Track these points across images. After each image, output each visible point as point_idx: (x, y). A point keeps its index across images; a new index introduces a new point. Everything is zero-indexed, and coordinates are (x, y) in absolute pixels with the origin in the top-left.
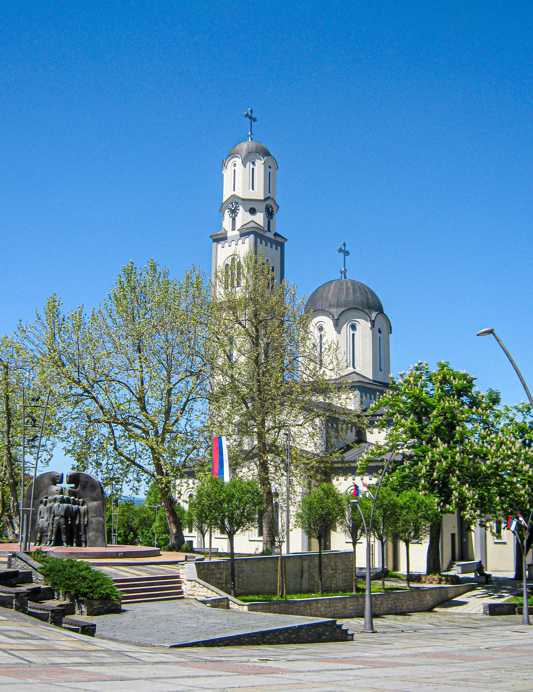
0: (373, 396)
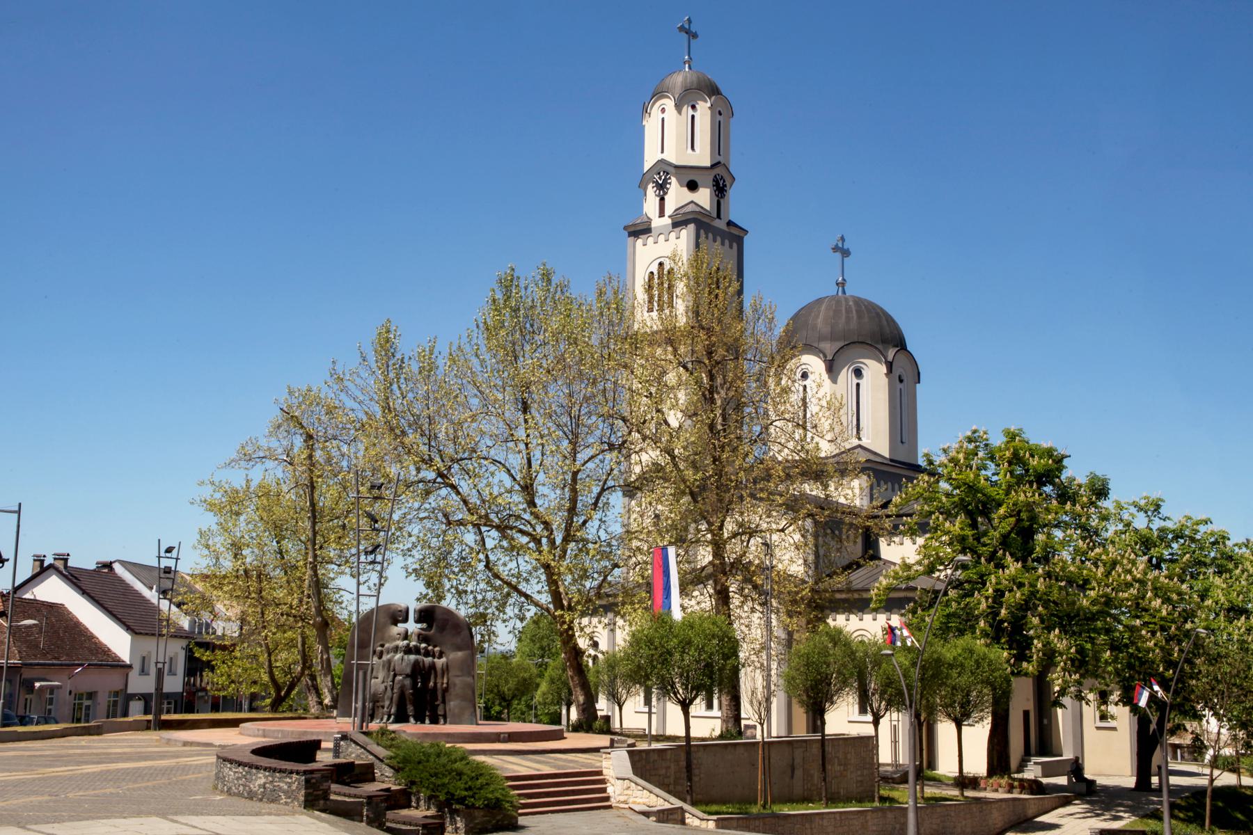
0: (897, 486)
